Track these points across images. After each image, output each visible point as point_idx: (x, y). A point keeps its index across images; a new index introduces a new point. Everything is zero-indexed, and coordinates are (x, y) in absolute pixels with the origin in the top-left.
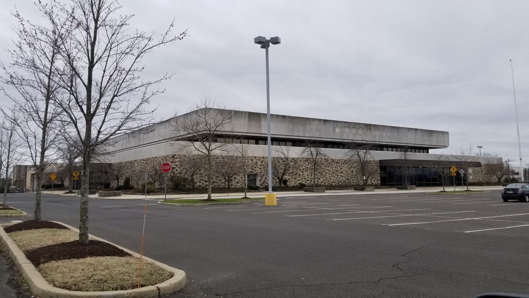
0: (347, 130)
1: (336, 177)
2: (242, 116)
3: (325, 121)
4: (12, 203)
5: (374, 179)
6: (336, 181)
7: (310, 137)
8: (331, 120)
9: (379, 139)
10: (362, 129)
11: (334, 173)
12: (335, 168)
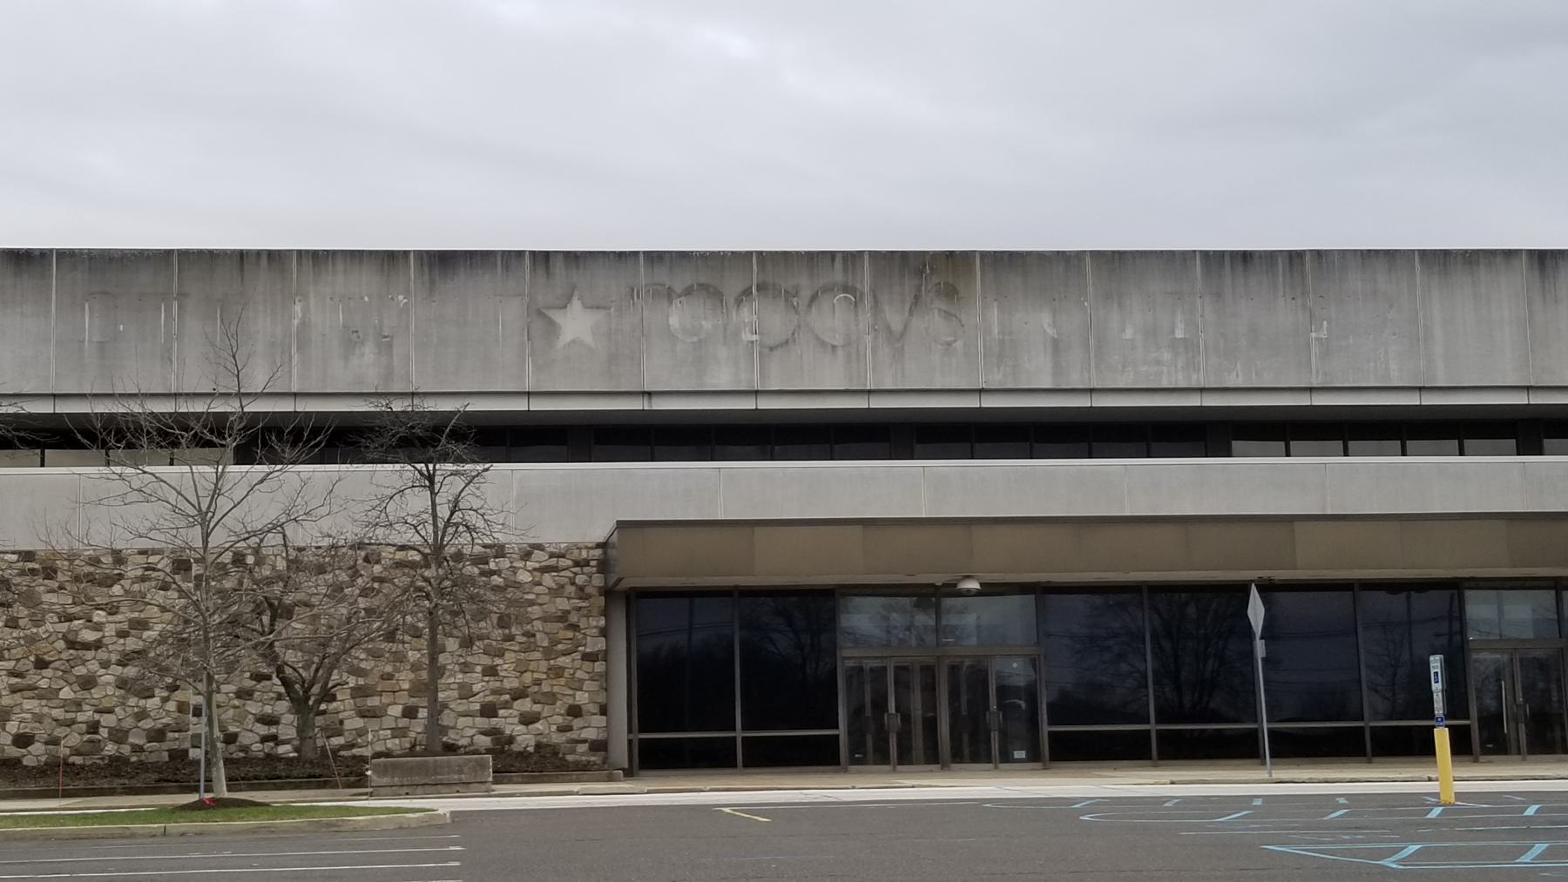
1: (66, 693)
3: (443, 263)
5: (525, 705)
6: (60, 732)
8: (1184, 253)
9: (1057, 370)
11: (41, 664)
12: (64, 627)
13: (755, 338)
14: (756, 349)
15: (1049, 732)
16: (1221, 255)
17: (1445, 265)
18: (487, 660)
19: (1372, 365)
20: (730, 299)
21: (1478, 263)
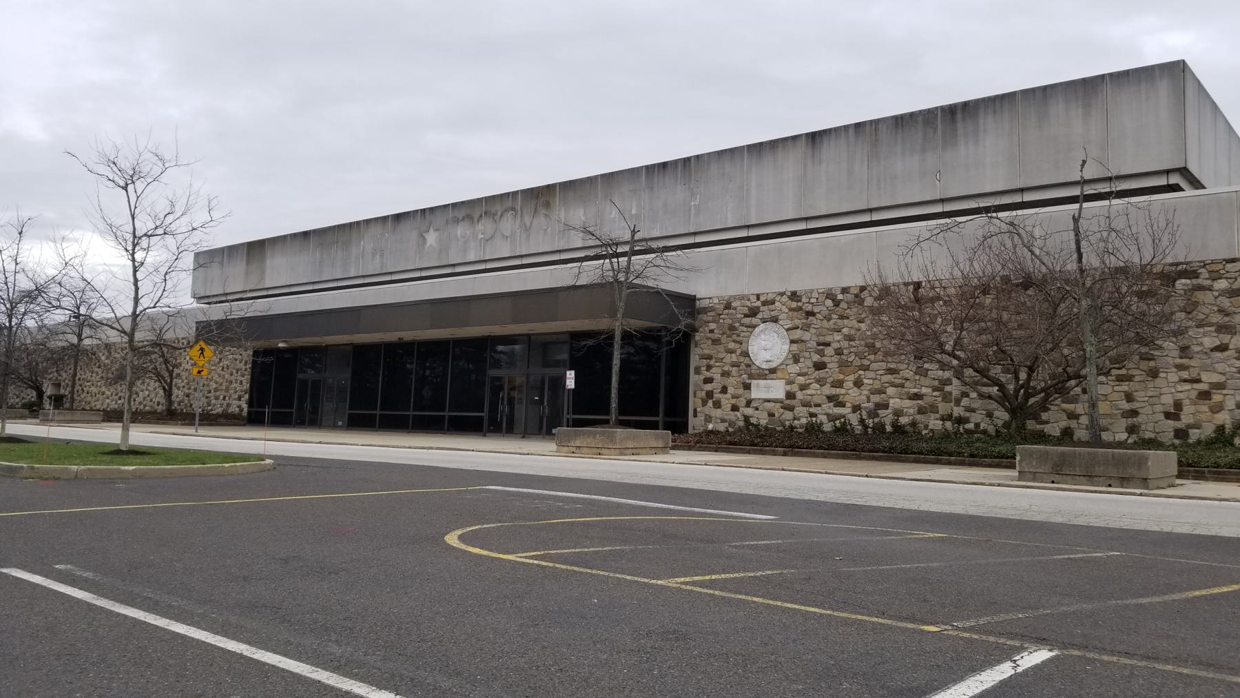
0: (460, 230)
2: (237, 252)
3: (398, 217)
4: (176, 469)
7: (806, 219)
10: (516, 213)
13: (483, 236)
14: (483, 241)
15: (658, 416)
16: (653, 166)
17: (760, 151)
18: (1145, 365)
19: (719, 216)
20: (476, 220)
21: (777, 147)
